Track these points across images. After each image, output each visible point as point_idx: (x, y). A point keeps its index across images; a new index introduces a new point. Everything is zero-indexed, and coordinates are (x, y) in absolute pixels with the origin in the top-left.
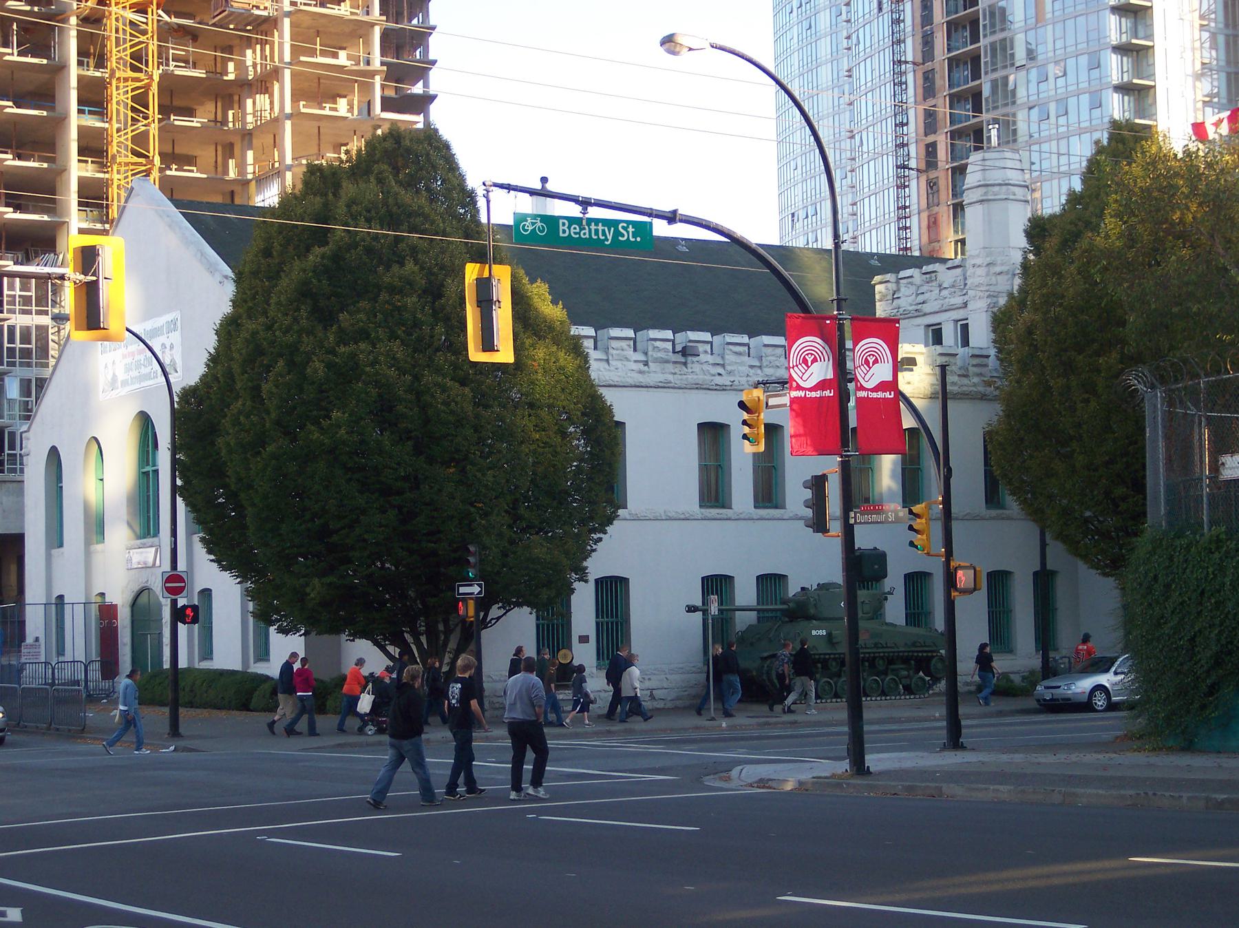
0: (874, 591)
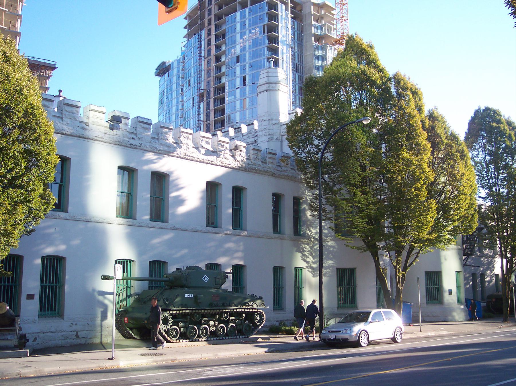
0: (216, 271)
